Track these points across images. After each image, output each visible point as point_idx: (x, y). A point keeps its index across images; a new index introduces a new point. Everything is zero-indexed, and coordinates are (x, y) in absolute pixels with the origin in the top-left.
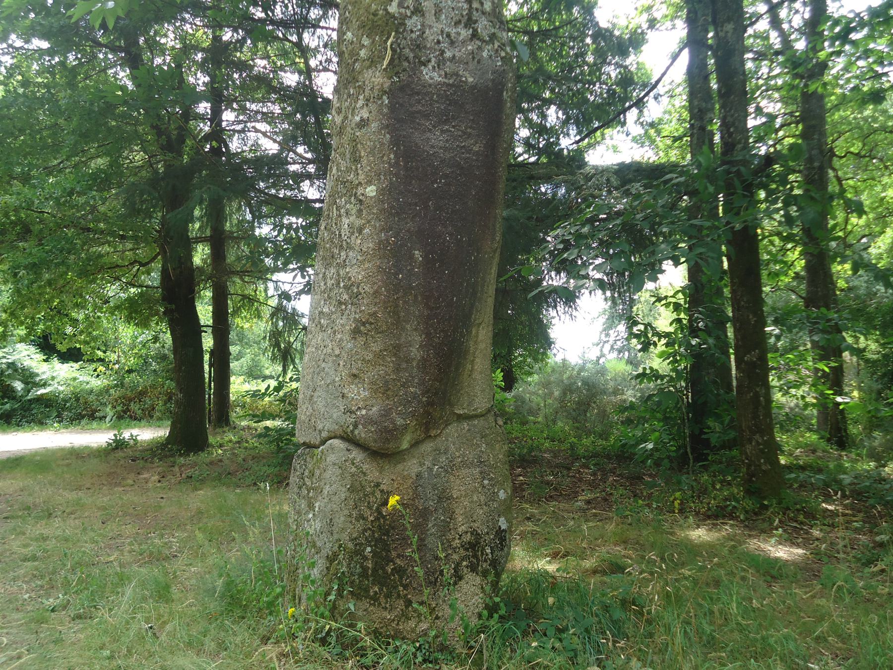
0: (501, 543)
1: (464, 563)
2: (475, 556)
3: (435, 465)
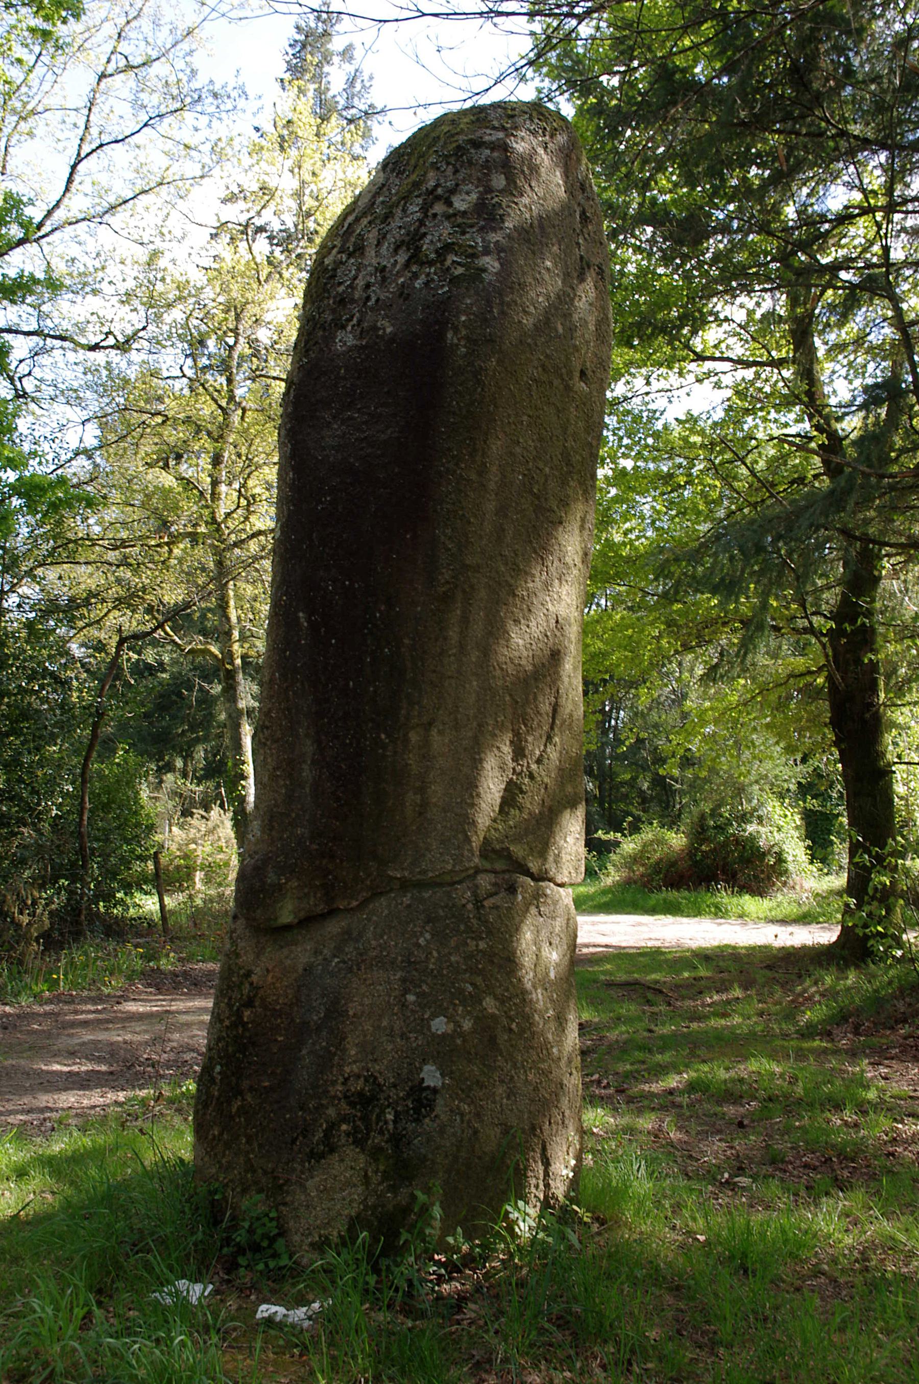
0: (417, 1110)
1: (344, 1127)
2: (365, 1118)
3: (335, 956)
